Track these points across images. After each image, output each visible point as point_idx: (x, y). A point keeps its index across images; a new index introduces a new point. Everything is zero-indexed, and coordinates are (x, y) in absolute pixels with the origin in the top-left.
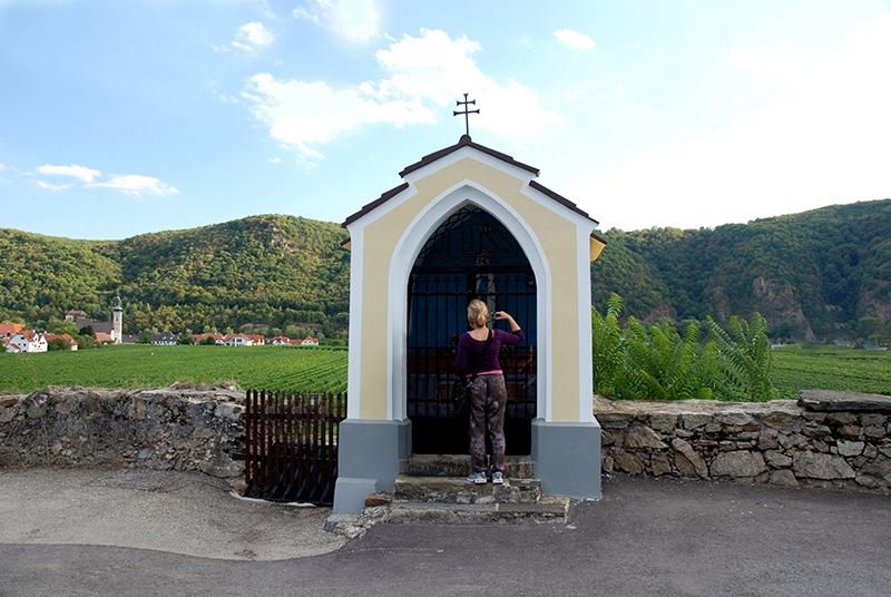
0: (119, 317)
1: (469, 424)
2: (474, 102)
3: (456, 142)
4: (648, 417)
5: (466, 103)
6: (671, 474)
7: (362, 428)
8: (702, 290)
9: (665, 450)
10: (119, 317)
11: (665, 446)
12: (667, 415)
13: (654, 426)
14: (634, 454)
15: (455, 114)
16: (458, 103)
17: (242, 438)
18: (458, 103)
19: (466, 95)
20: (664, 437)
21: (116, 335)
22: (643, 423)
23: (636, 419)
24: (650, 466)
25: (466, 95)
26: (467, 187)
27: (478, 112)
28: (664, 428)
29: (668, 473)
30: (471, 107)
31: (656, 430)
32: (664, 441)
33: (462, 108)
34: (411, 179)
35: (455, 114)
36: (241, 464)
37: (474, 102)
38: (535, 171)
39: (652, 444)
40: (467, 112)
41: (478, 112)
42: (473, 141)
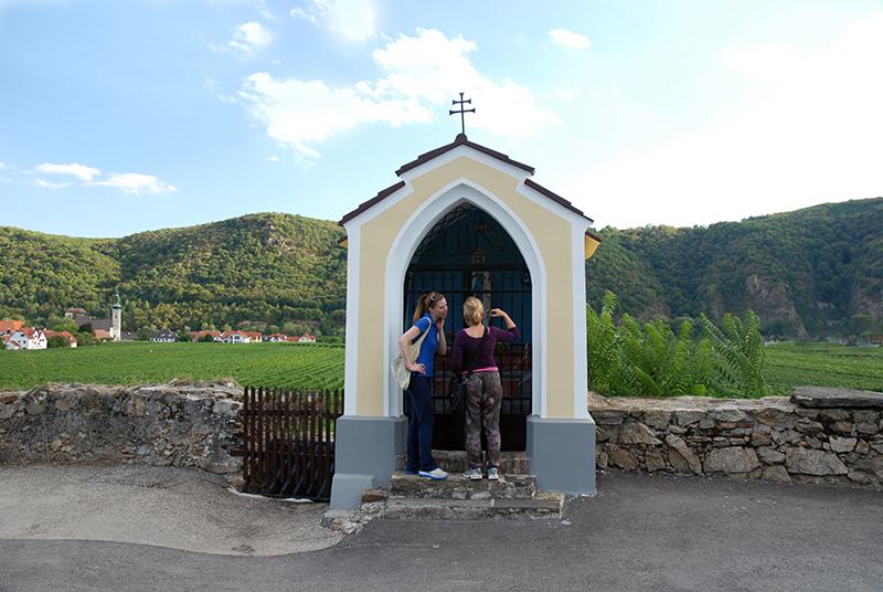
0: (118, 314)
2: (469, 102)
4: (643, 413)
5: (462, 102)
7: (358, 424)
9: (659, 446)
10: (118, 314)
11: (659, 442)
12: (661, 412)
15: (451, 113)
16: (454, 102)
17: (240, 435)
18: (454, 102)
19: (462, 95)
20: (658, 433)
21: (115, 333)
25: (462, 95)
27: (473, 111)
30: (467, 106)
32: (658, 437)
33: (458, 107)
35: (451, 113)
36: (239, 460)
37: (469, 102)
38: (531, 170)
39: (646, 441)
40: (462, 112)
41: (473, 111)
42: (469, 139)
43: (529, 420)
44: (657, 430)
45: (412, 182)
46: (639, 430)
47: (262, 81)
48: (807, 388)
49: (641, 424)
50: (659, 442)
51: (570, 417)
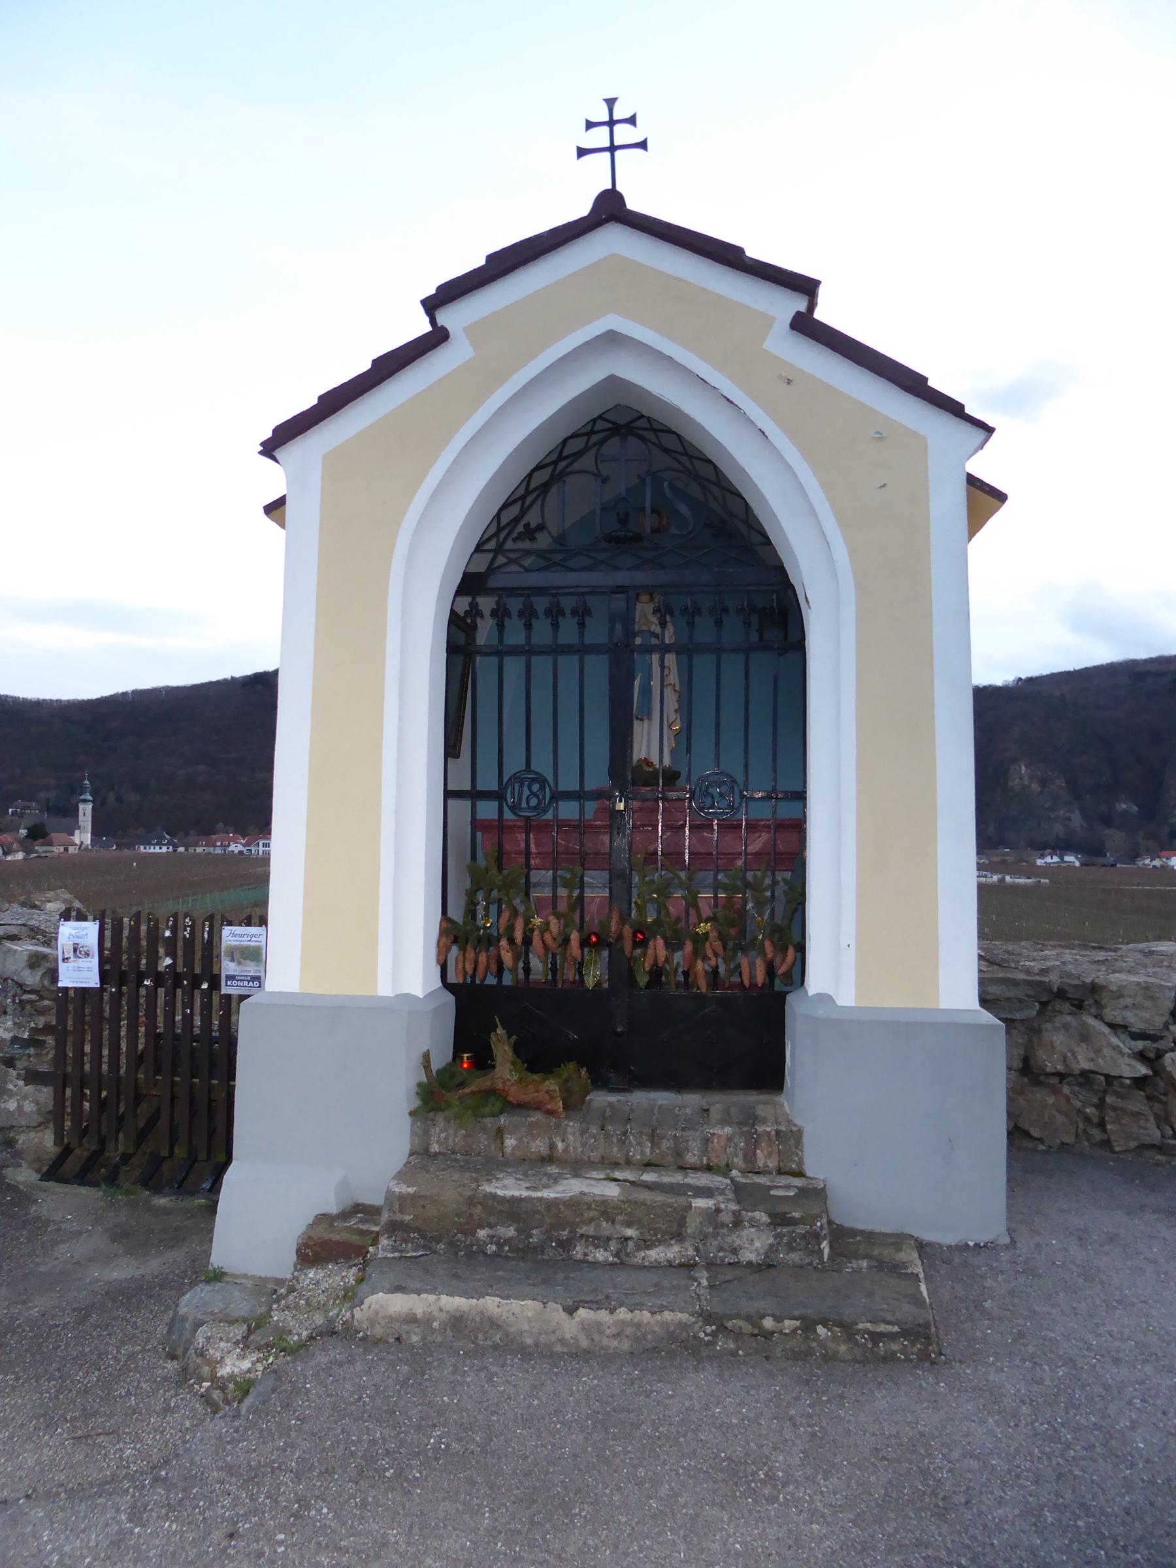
0: (86, 811)
1: (148, 945)
2: (632, 121)
3: (582, 209)
4: (1094, 988)
5: (611, 123)
6: (1160, 1149)
7: (290, 1005)
8: (652, 1143)
9: (1139, 1082)
10: (86, 811)
11: (1143, 1070)
12: (1147, 988)
13: (1111, 1014)
14: (1055, 1091)
15: (582, 152)
16: (590, 125)
17: (47, 1029)
18: (590, 125)
19: (611, 102)
20: (1140, 1045)
21: (83, 836)
22: (1079, 1005)
23: (1061, 994)
24: (1102, 1125)
25: (611, 102)
26: (612, 340)
27: (643, 145)
28: (1136, 1020)
29: (1152, 1146)
30: (623, 134)
31: (1113, 1026)
32: (1141, 1056)
33: (600, 137)
34: (445, 317)
35: (582, 152)
36: (46, 1094)
37: (632, 121)
38: (807, 287)
39: (1102, 1065)
40: (612, 149)
41: (643, 145)
42: (632, 204)
43: (795, 1006)
44: (1135, 1036)
45: (469, 330)
46: (1085, 1037)
47: (497, 599)
48: (1009, 994)
49: (1091, 1021)
50: (1143, 1070)
51: (927, 1005)
